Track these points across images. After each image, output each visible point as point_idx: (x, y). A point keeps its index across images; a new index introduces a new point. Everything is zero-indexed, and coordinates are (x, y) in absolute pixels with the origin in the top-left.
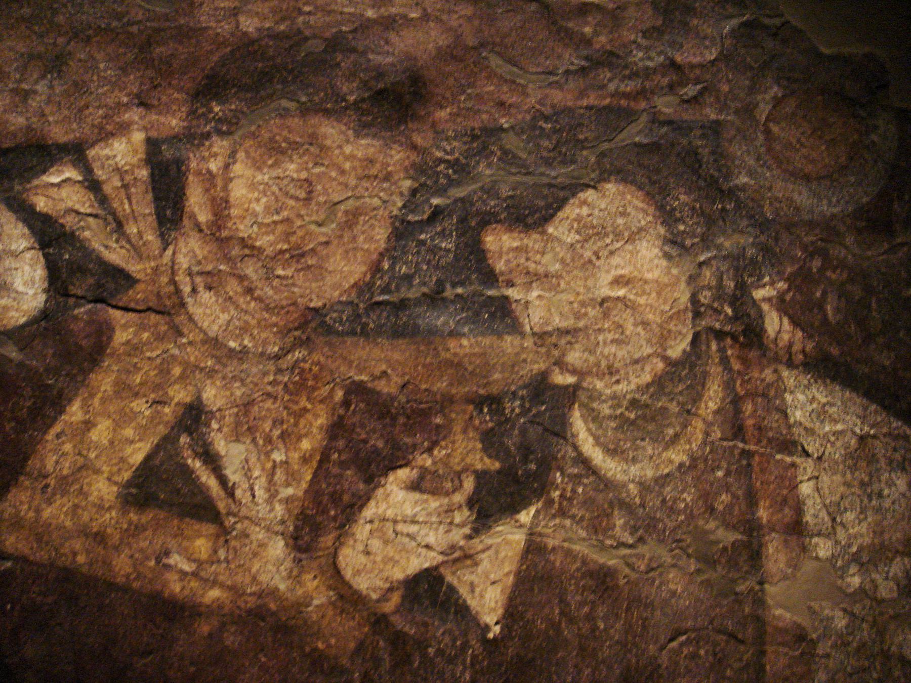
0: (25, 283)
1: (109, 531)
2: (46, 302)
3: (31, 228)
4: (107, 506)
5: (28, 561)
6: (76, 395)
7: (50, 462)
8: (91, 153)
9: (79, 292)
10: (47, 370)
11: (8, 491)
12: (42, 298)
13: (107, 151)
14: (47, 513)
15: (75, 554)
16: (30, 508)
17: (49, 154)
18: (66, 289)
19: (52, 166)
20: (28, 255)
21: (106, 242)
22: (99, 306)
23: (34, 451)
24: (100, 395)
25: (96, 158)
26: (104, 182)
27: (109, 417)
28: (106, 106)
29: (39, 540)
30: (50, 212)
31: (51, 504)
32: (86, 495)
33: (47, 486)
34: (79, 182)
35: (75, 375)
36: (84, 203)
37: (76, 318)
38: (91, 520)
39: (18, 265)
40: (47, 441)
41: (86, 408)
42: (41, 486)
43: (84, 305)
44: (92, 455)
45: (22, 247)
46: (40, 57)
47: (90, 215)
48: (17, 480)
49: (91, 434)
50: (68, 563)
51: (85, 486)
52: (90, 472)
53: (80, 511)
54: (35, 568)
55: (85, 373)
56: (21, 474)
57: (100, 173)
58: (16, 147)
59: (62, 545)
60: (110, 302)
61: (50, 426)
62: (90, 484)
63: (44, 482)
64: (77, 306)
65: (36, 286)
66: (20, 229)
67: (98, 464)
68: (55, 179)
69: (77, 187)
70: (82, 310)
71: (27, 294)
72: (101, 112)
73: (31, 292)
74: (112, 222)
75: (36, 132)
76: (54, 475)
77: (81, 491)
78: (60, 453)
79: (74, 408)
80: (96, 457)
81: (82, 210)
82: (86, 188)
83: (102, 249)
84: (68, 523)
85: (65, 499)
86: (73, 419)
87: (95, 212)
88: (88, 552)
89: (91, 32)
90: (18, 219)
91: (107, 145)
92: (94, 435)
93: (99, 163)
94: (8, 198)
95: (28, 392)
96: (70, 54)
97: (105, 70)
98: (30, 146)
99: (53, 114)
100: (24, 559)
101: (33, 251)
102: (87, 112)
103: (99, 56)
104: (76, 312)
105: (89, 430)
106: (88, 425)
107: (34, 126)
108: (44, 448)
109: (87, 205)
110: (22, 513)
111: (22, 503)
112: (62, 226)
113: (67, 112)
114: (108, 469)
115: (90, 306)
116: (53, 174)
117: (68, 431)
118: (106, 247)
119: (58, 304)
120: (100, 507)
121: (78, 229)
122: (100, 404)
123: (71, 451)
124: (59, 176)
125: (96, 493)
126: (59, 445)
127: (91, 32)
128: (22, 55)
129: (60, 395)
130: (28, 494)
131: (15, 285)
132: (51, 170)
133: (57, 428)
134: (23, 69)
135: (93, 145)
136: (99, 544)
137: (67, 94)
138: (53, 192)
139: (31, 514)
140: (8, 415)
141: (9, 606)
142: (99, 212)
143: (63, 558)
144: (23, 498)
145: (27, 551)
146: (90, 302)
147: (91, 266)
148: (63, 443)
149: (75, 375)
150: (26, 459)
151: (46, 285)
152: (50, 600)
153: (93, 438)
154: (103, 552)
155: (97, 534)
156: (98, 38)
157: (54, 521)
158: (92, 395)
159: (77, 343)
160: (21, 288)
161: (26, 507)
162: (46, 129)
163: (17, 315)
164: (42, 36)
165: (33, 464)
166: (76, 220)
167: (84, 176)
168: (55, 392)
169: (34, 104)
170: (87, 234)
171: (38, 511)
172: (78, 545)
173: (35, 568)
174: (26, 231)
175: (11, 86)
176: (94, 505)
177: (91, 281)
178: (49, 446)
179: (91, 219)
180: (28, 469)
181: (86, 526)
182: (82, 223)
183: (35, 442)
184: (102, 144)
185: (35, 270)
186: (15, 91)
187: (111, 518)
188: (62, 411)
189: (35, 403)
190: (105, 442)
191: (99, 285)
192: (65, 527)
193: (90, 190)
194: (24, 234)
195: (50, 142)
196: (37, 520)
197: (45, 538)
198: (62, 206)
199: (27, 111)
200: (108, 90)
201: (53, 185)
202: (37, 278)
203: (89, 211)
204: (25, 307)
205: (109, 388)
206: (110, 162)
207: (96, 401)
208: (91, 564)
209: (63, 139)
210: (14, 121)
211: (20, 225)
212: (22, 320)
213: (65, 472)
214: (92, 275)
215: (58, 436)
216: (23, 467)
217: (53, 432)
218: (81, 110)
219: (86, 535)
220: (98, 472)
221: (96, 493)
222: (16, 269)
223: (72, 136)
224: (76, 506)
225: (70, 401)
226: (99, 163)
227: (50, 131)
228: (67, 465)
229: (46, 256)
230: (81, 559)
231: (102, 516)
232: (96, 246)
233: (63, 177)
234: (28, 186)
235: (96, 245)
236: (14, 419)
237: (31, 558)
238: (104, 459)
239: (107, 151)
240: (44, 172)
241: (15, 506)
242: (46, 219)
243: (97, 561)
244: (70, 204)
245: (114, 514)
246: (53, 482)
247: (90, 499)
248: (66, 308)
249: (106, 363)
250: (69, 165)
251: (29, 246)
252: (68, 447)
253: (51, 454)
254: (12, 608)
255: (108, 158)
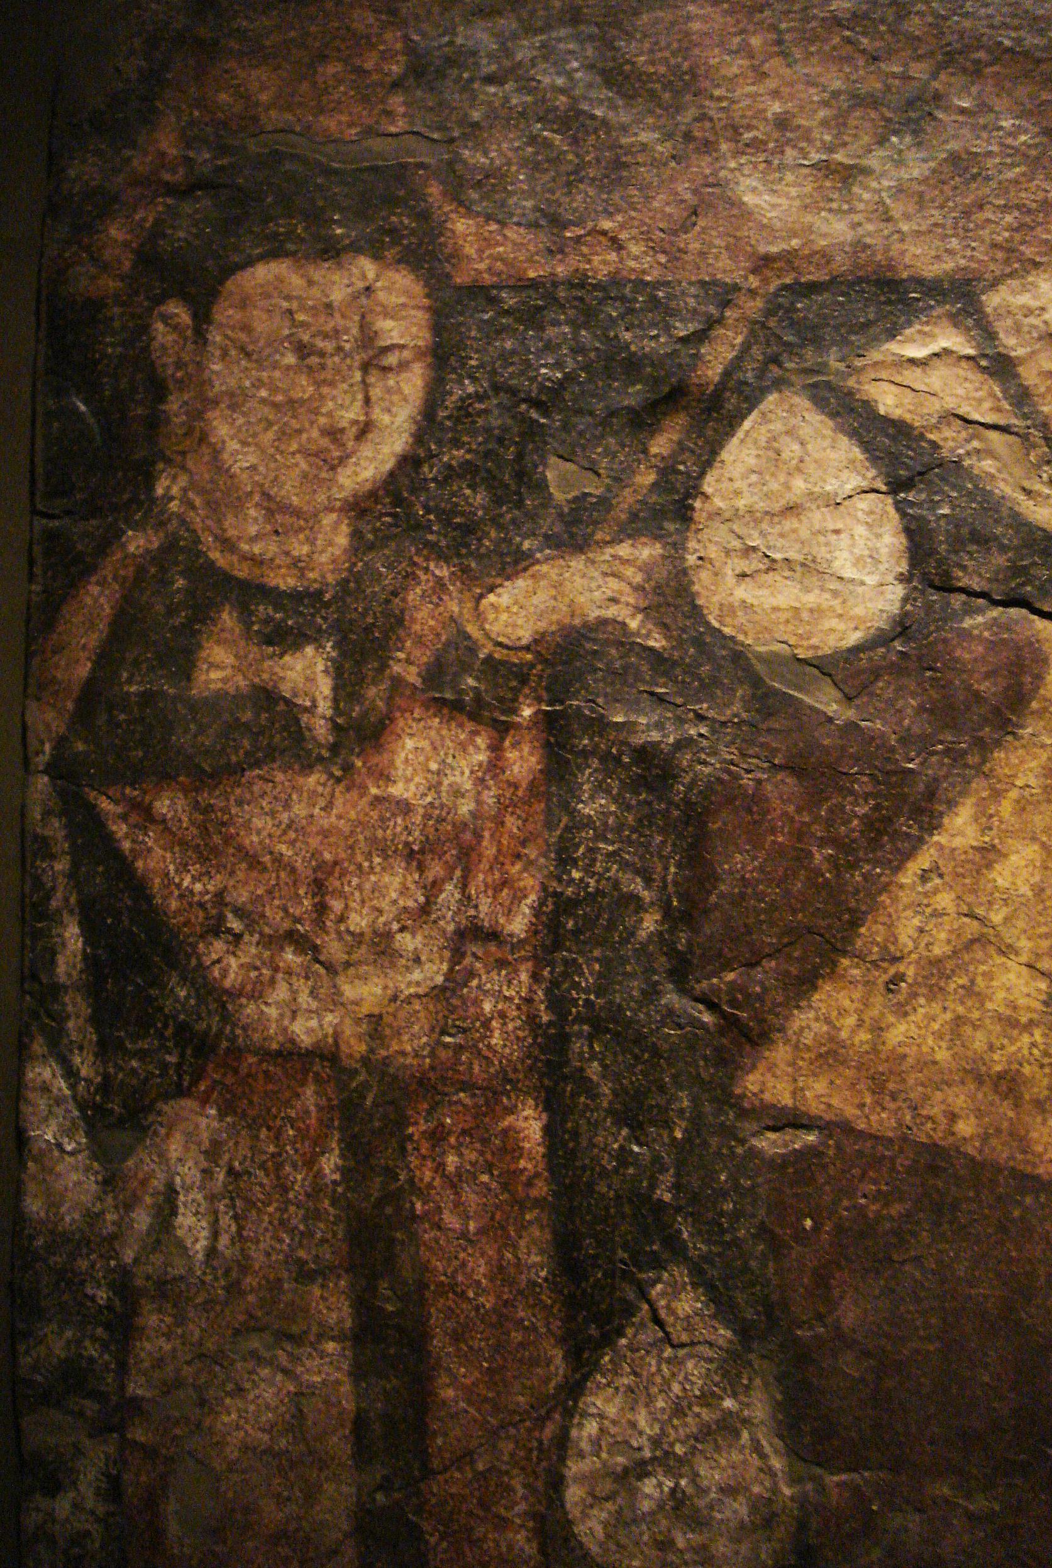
0: (858, 561)
1: (1027, 1070)
2: (905, 600)
3: (867, 446)
4: (1024, 1020)
5: (853, 1130)
6: (964, 793)
7: (907, 929)
8: (992, 301)
9: (976, 584)
10: (904, 741)
11: (815, 988)
12: (898, 591)
13: (1025, 299)
14: (898, 1033)
15: (953, 1117)
16: (860, 1023)
17: (905, 301)
18: (947, 575)
19: (909, 324)
20: (864, 504)
21: (1027, 484)
22: (1013, 611)
23: (874, 907)
24: (1014, 794)
25: (1002, 311)
26: (1021, 361)
27: (1034, 839)
28: (1018, 207)
29: (878, 1087)
30: (908, 417)
31: (906, 1014)
32: (981, 998)
33: (899, 978)
34: (969, 358)
35: (965, 752)
36: (980, 401)
37: (966, 635)
38: (991, 1048)
39: (840, 526)
40: (901, 886)
41: (984, 818)
42: (885, 977)
43: (980, 611)
44: (997, 918)
45: (848, 488)
46: (871, 102)
47: (995, 427)
48: (835, 964)
49: (993, 875)
50: (938, 1136)
51: (979, 980)
52: (992, 950)
53: (968, 1030)
54: (869, 1144)
55: (984, 747)
56: (844, 953)
57: (1011, 341)
58: (833, 280)
59: (926, 1098)
60: (1038, 605)
61: (909, 855)
62: (989, 976)
63: (892, 971)
64: (969, 611)
65: (882, 568)
66: (848, 450)
67: (1009, 935)
68: (918, 352)
69: (964, 370)
70: (980, 619)
71: (863, 583)
72: (1009, 218)
73: (871, 580)
74: (1042, 442)
75: (874, 254)
76: (913, 956)
77: (970, 990)
78: (928, 910)
79: (959, 821)
80: (1007, 920)
81: (976, 416)
82: (984, 370)
83: (1021, 497)
84: (942, 1055)
85: (936, 1008)
86: (958, 842)
87: (1002, 422)
88: (979, 1114)
89: (981, 55)
90: (841, 429)
91: (1024, 289)
92: (1001, 876)
93: (1009, 322)
94: (815, 386)
95: (862, 785)
96: (937, 97)
97: (1013, 134)
98: (860, 280)
99: (907, 217)
100: (846, 1128)
101: (873, 496)
102: (980, 216)
103: (1000, 104)
104: (967, 623)
105: (989, 866)
106: (989, 854)
107: (868, 240)
108: (895, 900)
109: (987, 405)
110: (844, 1035)
111: (842, 1012)
112: (935, 446)
113: (937, 215)
114: (1030, 944)
115: (995, 612)
116: (911, 340)
117: (946, 868)
118: (1028, 492)
119: (929, 607)
120: (1011, 1023)
121: (968, 454)
122: (1012, 814)
123: (951, 909)
124: (925, 345)
125: (1001, 995)
126: (926, 894)
127: (981, 55)
128: (836, 94)
129: (931, 794)
130: (856, 995)
131: (837, 564)
132: (908, 332)
133: (923, 860)
134: (839, 122)
135: (994, 284)
136: (1006, 1097)
137: (936, 179)
138: (911, 376)
139: (864, 1036)
140: (818, 831)
141: (808, 1223)
142: (1014, 421)
143: (929, 1125)
144: (847, 1003)
145: (851, 1112)
146: (996, 603)
147: (999, 530)
148: (936, 891)
149: (965, 752)
150: (855, 923)
151: (903, 567)
152: (896, 1209)
153: (1000, 882)
154: (1011, 1114)
155: (1001, 1076)
156: (996, 68)
157: (912, 1051)
158: (997, 795)
159: (969, 688)
160: (849, 573)
161: (851, 1021)
162: (896, 247)
163: (842, 627)
164: (875, 59)
165: (871, 933)
166: (964, 434)
167: (978, 346)
168: (921, 787)
169: (866, 196)
170: (987, 465)
171: (878, 1029)
172: (959, 1099)
173: (869, 1144)
174: (857, 453)
175: (815, 157)
176: (1000, 1018)
177: (1000, 560)
178: (905, 897)
179: (993, 435)
180: (859, 943)
181: (979, 1059)
182: (976, 444)
183: (875, 889)
184: (1014, 283)
185: (878, 536)
186: (825, 169)
187: (1034, 1045)
188: (934, 827)
189: (877, 807)
190: (1025, 890)
191: (1016, 570)
192: (935, 1063)
193: (991, 375)
194: (852, 462)
195: (905, 275)
196: (875, 1050)
197: (891, 1086)
198: (934, 406)
199: (852, 210)
200: (1024, 174)
201: (912, 361)
202: (884, 551)
203: (989, 419)
204: (859, 611)
205: (1033, 782)
206: (1032, 320)
207: (1006, 807)
208: (985, 1138)
209: (932, 271)
210: (824, 229)
211: (844, 441)
212: (854, 638)
213: (937, 951)
214: (1003, 549)
215: (924, 876)
216: (848, 940)
217: (914, 867)
218: (967, 214)
219: (979, 1080)
220: (1007, 950)
221: (1001, 995)
222: (837, 532)
223: (949, 265)
224: (959, 1021)
225: (951, 804)
226: (1009, 322)
227: (903, 253)
228: (943, 936)
229: (899, 506)
230: (965, 1128)
231: (1013, 1041)
232: (1008, 490)
233: (935, 347)
234: (858, 363)
235: (1004, 488)
236: (834, 841)
237: (862, 1126)
238: (1021, 924)
239: (1025, 299)
240: (892, 334)
241: (828, 1021)
242: (900, 429)
243: (998, 1131)
244: (950, 403)
245: (1038, 1036)
246: (911, 972)
247: (989, 1005)
248: (948, 616)
249: (1029, 730)
250: (945, 322)
251: (865, 484)
252: (945, 900)
253: (909, 913)
254: (817, 1228)
255: (1029, 312)
